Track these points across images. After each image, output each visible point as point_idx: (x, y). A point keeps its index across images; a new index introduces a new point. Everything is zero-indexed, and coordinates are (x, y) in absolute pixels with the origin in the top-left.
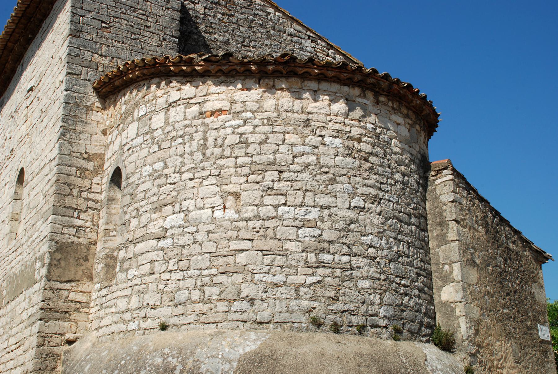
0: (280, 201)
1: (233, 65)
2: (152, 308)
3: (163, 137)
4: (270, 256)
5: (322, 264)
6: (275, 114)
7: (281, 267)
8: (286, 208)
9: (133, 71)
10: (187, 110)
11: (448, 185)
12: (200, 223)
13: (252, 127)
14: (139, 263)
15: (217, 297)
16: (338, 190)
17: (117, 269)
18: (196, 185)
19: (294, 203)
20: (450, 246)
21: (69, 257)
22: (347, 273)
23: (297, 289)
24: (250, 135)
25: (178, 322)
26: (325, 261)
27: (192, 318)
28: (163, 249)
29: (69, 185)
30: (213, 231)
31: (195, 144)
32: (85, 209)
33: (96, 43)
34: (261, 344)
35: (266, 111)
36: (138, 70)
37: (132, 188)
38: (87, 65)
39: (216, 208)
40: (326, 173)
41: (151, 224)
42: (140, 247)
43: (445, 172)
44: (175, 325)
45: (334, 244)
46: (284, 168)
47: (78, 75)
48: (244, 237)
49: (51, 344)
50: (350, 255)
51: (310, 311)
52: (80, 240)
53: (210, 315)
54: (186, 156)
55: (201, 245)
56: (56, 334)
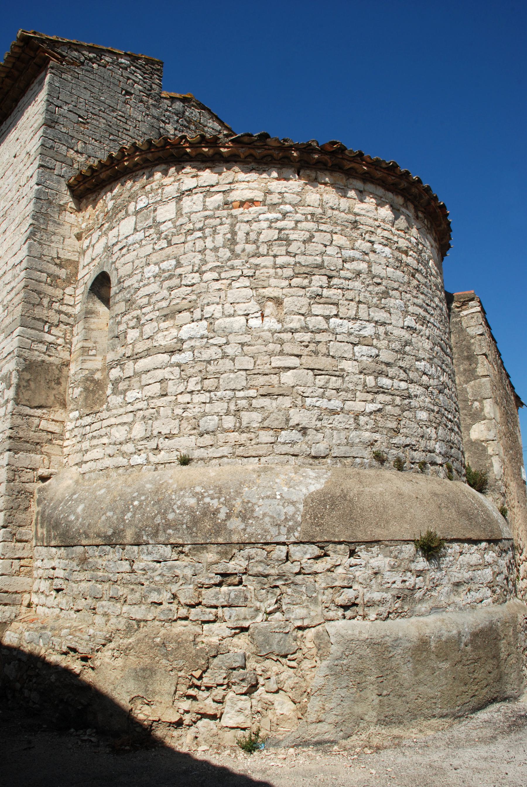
0: (331, 312)
1: (269, 149)
2: (166, 438)
3: (174, 230)
4: (323, 376)
5: (382, 390)
6: (320, 211)
7: (337, 390)
8: (338, 321)
9: (131, 156)
10: (207, 199)
11: (475, 317)
12: (231, 333)
13: (293, 222)
14: (143, 383)
15: (258, 425)
16: (391, 305)
17: (109, 392)
18: (223, 287)
19: (348, 315)
20: (480, 382)
21: (39, 378)
22: (406, 402)
23: (356, 418)
24: (292, 231)
25: (205, 456)
26: (385, 386)
27: (225, 450)
28: (179, 365)
29: (39, 293)
30: (249, 343)
31: (220, 240)
32: (56, 322)
33: (72, 137)
34: (327, 482)
35: (309, 206)
36: (138, 156)
37: (129, 292)
38: (62, 160)
39: (251, 316)
40: (379, 284)
41: (160, 334)
42: (143, 364)
43: (471, 303)
44: (202, 459)
45: (391, 367)
46: (334, 273)
47: (51, 169)
48: (290, 352)
49: (23, 479)
50: (406, 381)
51: (372, 444)
52: (52, 359)
53: (251, 447)
54: (208, 252)
55: (233, 360)
56: (27, 468)
